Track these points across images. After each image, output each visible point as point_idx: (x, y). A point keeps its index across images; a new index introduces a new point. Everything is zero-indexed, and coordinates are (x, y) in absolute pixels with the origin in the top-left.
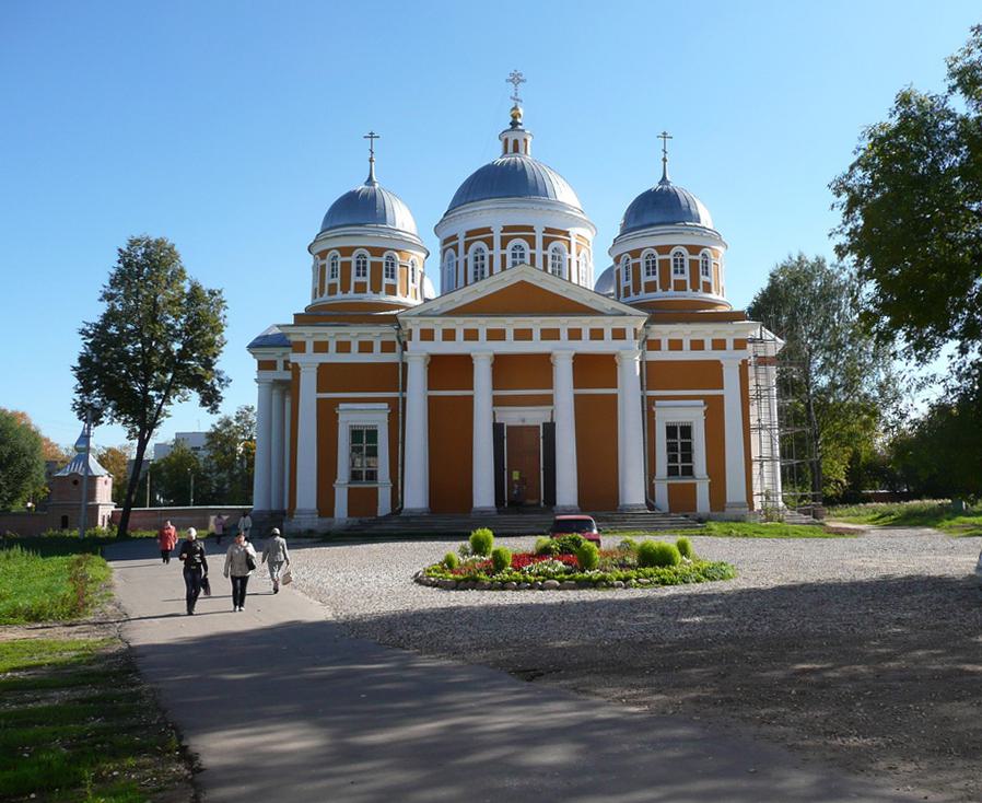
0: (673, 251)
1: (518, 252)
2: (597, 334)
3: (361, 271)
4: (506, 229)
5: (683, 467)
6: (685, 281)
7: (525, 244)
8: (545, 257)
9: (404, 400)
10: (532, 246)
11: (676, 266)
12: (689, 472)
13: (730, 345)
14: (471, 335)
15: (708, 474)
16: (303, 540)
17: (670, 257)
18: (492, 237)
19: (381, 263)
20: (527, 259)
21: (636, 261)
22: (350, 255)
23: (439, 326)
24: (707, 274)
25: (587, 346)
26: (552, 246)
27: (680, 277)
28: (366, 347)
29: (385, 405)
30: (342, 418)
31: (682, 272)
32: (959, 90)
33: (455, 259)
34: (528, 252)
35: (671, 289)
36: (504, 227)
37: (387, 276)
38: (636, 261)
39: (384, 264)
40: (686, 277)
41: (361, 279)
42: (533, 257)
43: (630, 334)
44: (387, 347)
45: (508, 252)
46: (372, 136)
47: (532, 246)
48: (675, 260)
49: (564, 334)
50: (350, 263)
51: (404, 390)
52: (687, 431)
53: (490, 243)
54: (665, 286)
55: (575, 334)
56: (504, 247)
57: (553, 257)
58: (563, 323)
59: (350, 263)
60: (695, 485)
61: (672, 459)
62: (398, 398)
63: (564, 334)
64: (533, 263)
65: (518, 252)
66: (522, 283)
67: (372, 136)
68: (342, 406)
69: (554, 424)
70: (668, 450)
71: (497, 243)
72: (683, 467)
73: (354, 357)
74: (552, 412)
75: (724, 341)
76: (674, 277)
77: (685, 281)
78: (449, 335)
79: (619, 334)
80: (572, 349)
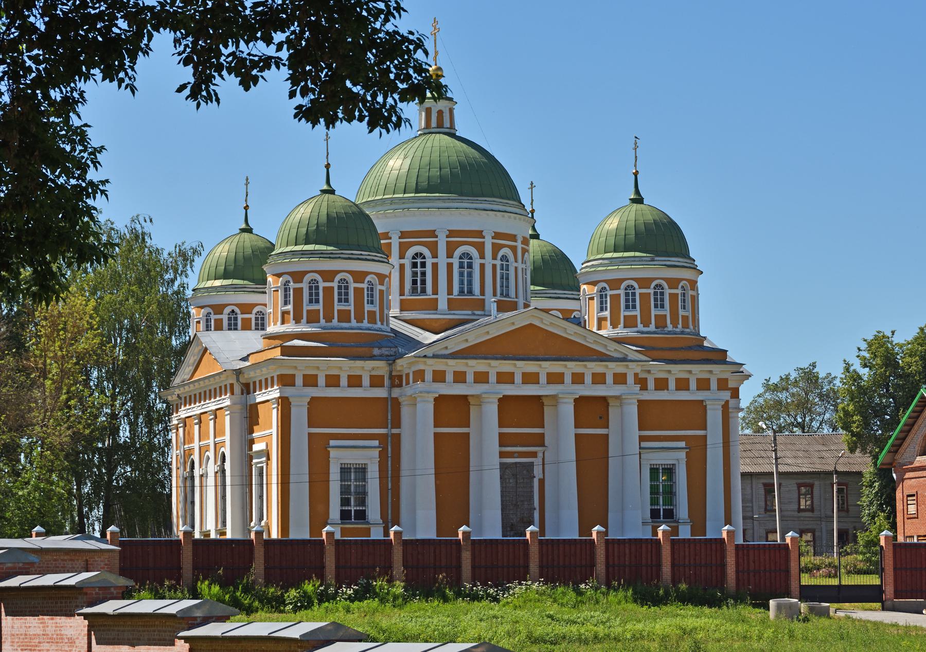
2: (599, 379)
3: (344, 299)
5: (355, 510)
12: (361, 515)
13: (299, 381)
14: (481, 378)
16: (90, 586)
19: (363, 289)
21: (298, 285)
22: (333, 281)
23: (452, 366)
24: (372, 303)
25: (589, 390)
28: (355, 382)
29: (376, 443)
30: (333, 453)
32: (290, 81)
38: (298, 285)
39: (366, 290)
41: (314, 307)
43: (630, 379)
44: (376, 382)
49: (568, 379)
50: (302, 289)
55: (578, 379)
58: (569, 368)
59: (302, 289)
61: (345, 502)
62: (387, 434)
63: (568, 379)
68: (332, 443)
70: (342, 493)
72: (355, 510)
73: (344, 392)
74: (544, 453)
75: (338, 377)
76: (337, 307)
78: (460, 378)
79: (620, 379)
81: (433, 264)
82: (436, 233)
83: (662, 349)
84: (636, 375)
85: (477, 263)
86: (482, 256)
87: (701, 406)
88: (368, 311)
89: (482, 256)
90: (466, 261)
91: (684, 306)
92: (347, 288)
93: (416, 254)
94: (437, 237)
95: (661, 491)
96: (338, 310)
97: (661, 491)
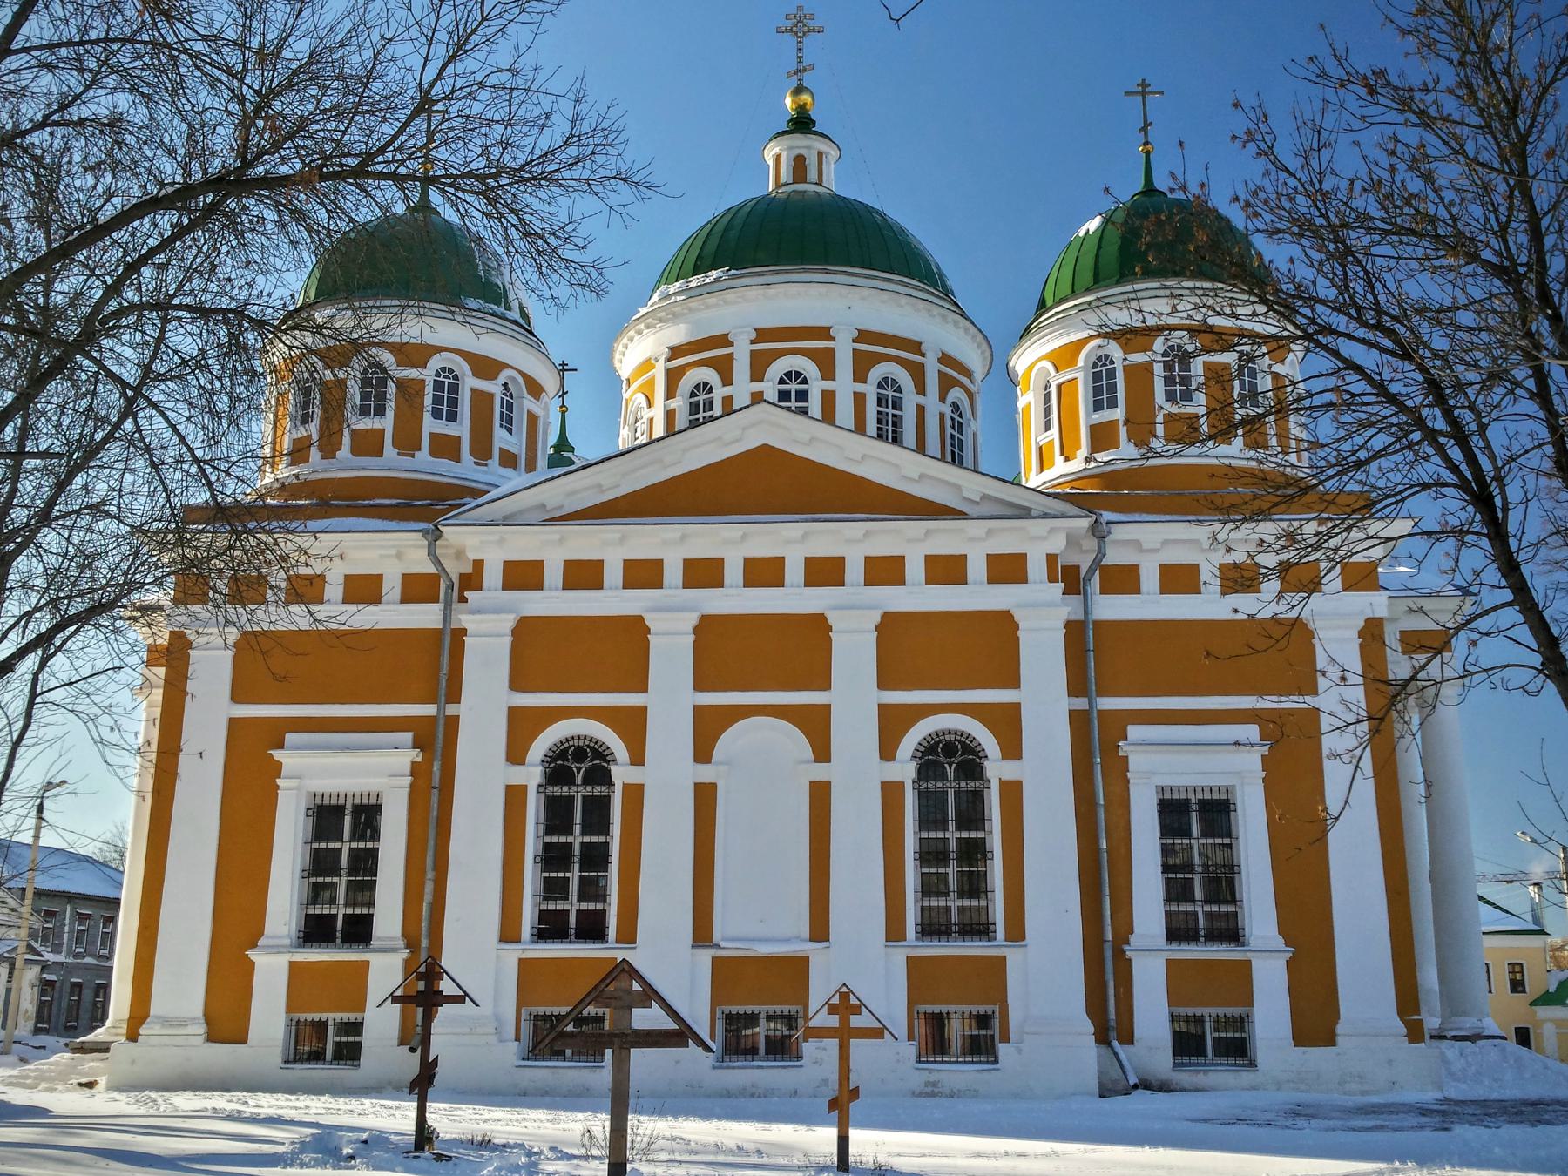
0: (436, 363)
1: (793, 387)
4: (762, 335)
6: (458, 439)
7: (809, 368)
8: (859, 399)
9: (453, 723)
10: (828, 372)
11: (437, 400)
12: (1230, 932)
14: (643, 574)
15: (1282, 931)
17: (428, 375)
18: (731, 357)
20: (815, 405)
26: (877, 372)
27: (444, 428)
28: (1179, 579)
31: (453, 417)
33: (647, 414)
34: (816, 387)
35: (423, 455)
36: (672, 349)
37: (437, 414)
39: (429, 389)
40: (461, 429)
42: (829, 398)
43: (1037, 567)
44: (417, 589)
45: (870, 390)
46: (1144, 89)
47: (828, 372)
48: (438, 386)
51: (454, 696)
52: (368, 815)
53: (725, 368)
54: (408, 442)
56: (757, 375)
57: (881, 401)
60: (1247, 964)
62: (1100, 694)
64: (829, 416)
65: (793, 387)
66: (765, 451)
67: (1144, 89)
69: (380, 807)
71: (742, 368)
73: (1211, 605)
77: (458, 439)
78: (584, 575)
79: (1007, 569)
80: (692, 610)
81: (824, 393)
82: (731, 338)
83: (487, 503)
84: (1052, 559)
85: (910, 400)
86: (921, 389)
87: (634, 631)
88: (432, 435)
89: (921, 389)
90: (890, 393)
91: (510, 420)
92: (454, 389)
93: (788, 374)
94: (732, 344)
95: (1194, 816)
96: (432, 435)
97: (1194, 816)
